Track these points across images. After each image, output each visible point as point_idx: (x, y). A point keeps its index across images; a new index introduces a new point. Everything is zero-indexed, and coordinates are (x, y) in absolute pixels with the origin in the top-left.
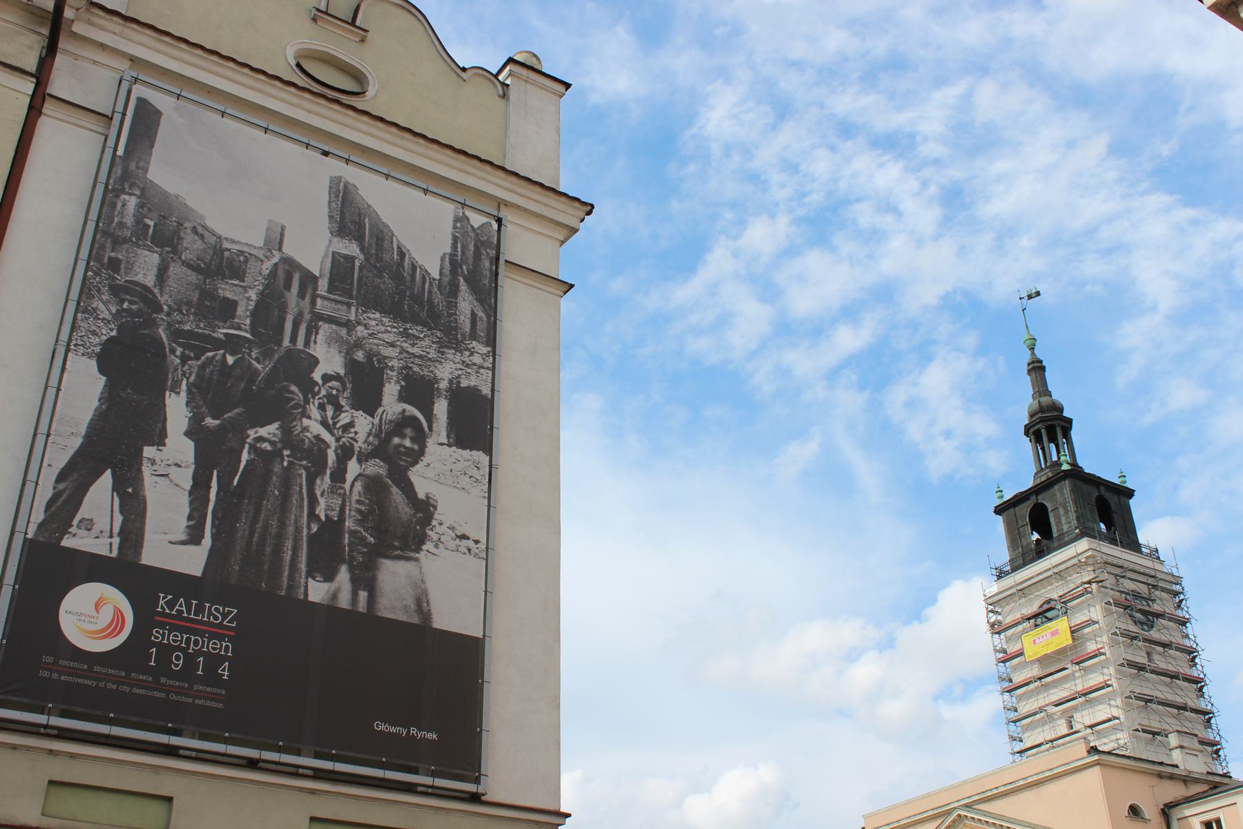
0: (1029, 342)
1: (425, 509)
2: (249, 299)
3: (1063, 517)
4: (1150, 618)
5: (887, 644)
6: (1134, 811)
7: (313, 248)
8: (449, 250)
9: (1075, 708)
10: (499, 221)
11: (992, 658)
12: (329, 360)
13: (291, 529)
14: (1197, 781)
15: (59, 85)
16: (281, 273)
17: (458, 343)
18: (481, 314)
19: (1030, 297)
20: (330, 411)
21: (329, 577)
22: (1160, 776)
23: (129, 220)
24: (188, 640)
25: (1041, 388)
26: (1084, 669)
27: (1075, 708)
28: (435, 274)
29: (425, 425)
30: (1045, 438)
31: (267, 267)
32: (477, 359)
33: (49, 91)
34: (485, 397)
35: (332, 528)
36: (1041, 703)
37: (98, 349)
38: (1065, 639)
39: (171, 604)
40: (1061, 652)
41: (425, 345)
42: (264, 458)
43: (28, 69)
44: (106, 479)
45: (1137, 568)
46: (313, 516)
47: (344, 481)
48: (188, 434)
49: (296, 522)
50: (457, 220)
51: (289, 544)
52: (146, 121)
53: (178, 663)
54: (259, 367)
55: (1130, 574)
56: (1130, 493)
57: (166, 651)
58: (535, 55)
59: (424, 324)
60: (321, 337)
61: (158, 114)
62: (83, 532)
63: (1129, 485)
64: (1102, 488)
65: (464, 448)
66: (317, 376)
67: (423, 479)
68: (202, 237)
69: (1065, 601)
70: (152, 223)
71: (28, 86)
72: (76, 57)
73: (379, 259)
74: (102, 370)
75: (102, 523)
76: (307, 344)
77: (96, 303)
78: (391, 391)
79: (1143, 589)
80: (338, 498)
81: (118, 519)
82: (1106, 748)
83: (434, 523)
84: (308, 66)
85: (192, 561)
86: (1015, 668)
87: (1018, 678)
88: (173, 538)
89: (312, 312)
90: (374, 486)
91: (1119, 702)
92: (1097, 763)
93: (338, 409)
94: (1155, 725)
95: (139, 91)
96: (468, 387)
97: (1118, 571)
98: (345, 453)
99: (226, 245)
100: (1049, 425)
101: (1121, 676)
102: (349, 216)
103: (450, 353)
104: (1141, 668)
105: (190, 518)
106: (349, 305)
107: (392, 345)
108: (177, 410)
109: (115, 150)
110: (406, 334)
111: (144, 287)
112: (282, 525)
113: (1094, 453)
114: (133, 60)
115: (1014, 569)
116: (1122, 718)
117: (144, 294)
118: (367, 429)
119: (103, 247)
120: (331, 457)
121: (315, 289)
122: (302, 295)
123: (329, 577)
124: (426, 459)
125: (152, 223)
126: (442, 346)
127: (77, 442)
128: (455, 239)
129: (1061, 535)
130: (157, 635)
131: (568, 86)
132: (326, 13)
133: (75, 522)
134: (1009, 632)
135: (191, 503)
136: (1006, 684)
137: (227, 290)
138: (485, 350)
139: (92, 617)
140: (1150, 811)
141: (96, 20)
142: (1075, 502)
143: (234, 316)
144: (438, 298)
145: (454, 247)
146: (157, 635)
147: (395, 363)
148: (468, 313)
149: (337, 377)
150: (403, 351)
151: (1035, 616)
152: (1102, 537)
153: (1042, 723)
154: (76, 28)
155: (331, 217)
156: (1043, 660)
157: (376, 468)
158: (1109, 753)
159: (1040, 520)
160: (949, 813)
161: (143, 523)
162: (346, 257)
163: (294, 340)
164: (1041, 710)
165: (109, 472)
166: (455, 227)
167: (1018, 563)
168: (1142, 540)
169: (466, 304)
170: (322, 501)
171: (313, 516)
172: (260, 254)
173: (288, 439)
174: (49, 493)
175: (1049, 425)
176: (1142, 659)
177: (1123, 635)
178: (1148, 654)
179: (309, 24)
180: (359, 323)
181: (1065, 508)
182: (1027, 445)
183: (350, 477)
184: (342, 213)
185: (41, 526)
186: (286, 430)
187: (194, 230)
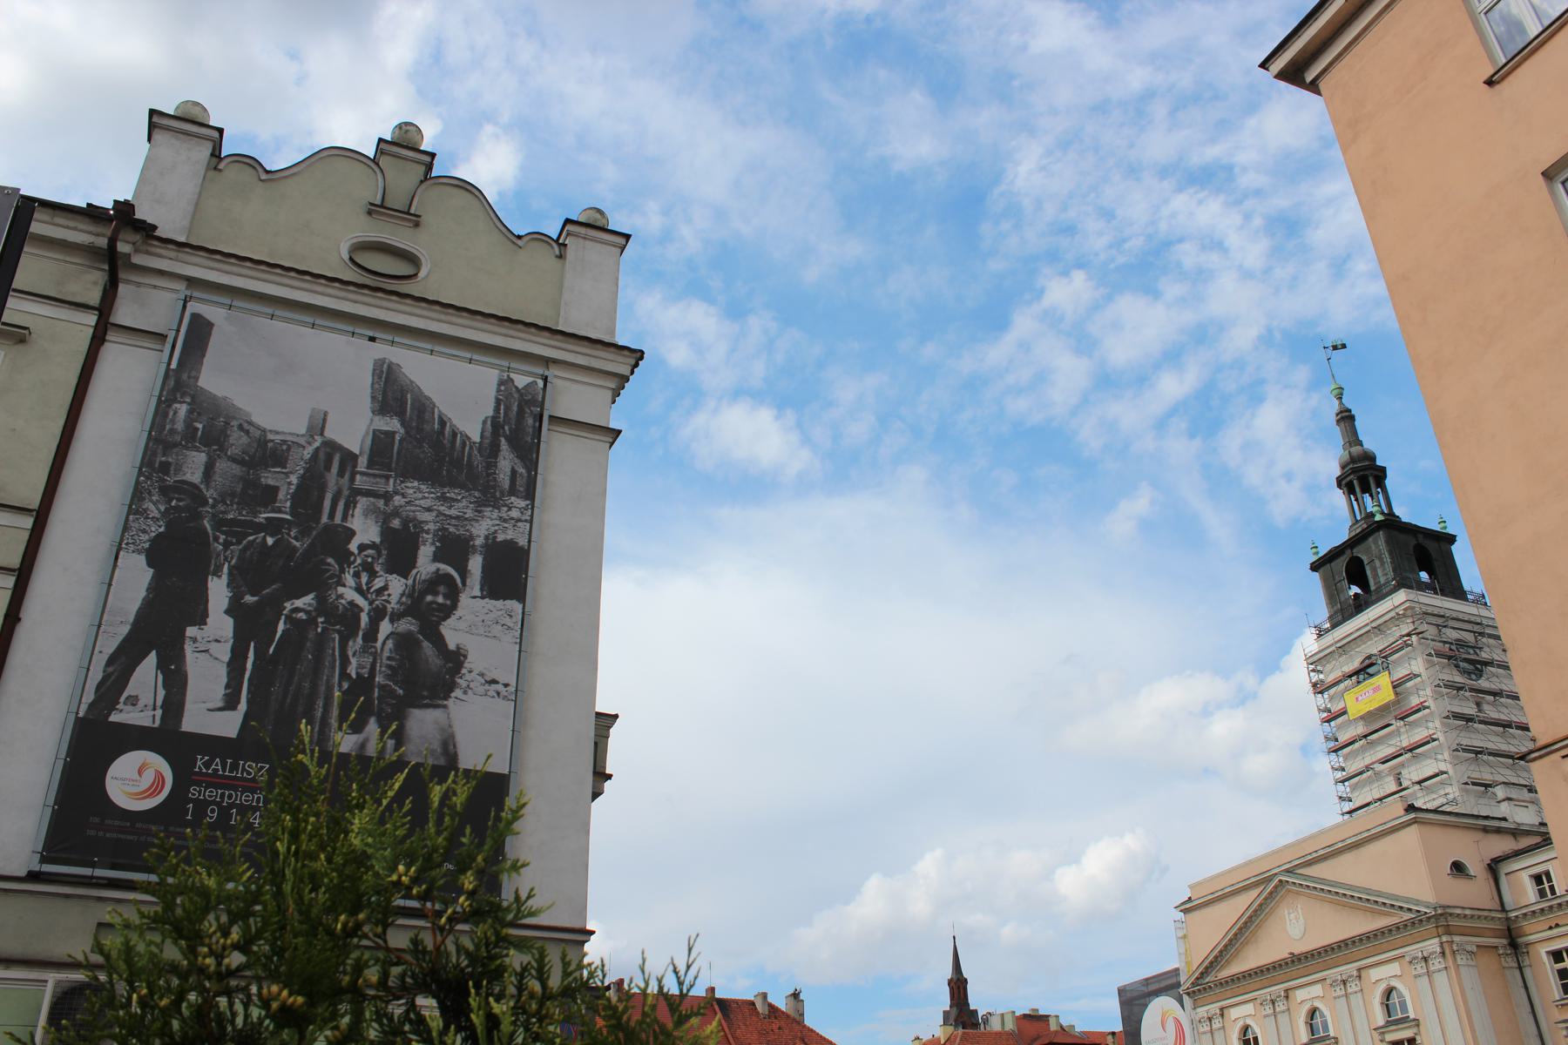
1: (456, 659)
2: (290, 483)
3: (1381, 570)
4: (1478, 667)
5: (1243, 698)
6: (1458, 868)
7: (353, 428)
8: (491, 413)
9: (1402, 765)
10: (545, 379)
11: (1317, 717)
12: (365, 530)
13: (323, 689)
14: (1528, 833)
15: (124, 314)
16: (322, 455)
17: (497, 500)
18: (522, 470)
19: (1335, 348)
20: (364, 578)
21: (357, 728)
22: (1485, 830)
23: (180, 426)
24: (223, 795)
25: (1352, 438)
26: (1410, 724)
27: (1402, 765)
28: (476, 438)
29: (458, 580)
30: (1358, 490)
31: (307, 453)
32: (515, 513)
33: (112, 320)
34: (522, 548)
35: (362, 685)
36: (1367, 761)
37: (147, 545)
38: (1387, 695)
39: (207, 765)
40: (1384, 709)
41: (463, 505)
42: (298, 628)
43: (91, 303)
44: (152, 658)
45: (1461, 616)
46: (344, 675)
47: (376, 640)
48: (227, 612)
49: (328, 681)
50: (501, 383)
51: (320, 703)
52: (199, 333)
53: (213, 815)
54: (297, 544)
55: (1451, 623)
56: (1451, 539)
57: (202, 806)
58: (598, 211)
59: (462, 486)
60: (358, 511)
61: (210, 325)
62: (129, 708)
63: (1450, 531)
64: (1420, 537)
65: (497, 599)
66: (353, 547)
67: (453, 633)
68: (247, 432)
69: (1385, 655)
70: (200, 426)
71: (91, 319)
72: (139, 284)
73: (420, 430)
74: (149, 564)
75: (146, 698)
76: (345, 518)
77: (148, 505)
78: (426, 552)
79: (1470, 637)
80: (367, 657)
81: (161, 693)
82: (1430, 806)
83: (464, 671)
84: (363, 259)
85: (228, 725)
86: (1339, 727)
87: (1344, 737)
88: (211, 705)
89: (350, 488)
90: (404, 643)
91: (1446, 755)
92: (1414, 821)
93: (373, 575)
94: (1487, 777)
95: (193, 307)
96: (505, 541)
97: (1440, 621)
98: (378, 615)
99: (270, 437)
100: (1363, 475)
101: (1447, 729)
102: (391, 393)
103: (487, 511)
104: (1469, 719)
105: (227, 687)
106: (387, 478)
107: (429, 510)
108: (218, 591)
109: (169, 364)
110: (443, 498)
111: (195, 486)
112: (314, 686)
113: (1412, 501)
114: (191, 282)
115: (1334, 626)
116: (1451, 772)
117: (192, 492)
118: (400, 591)
119: (154, 454)
120: (364, 618)
121: (355, 466)
122: (341, 474)
123: (357, 728)
124: (458, 613)
125: (200, 426)
126: (480, 505)
127: (126, 629)
128: (498, 402)
129: (1379, 588)
130: (194, 792)
131: (628, 237)
132: (382, 206)
133: (122, 699)
134: (1332, 691)
135: (229, 673)
136: (1332, 744)
137: (269, 478)
138: (523, 504)
139: (135, 781)
140: (1475, 866)
141: (153, 250)
142: (1391, 553)
143: (275, 501)
144: (478, 460)
145: (497, 409)
146: (194, 792)
147: (431, 527)
148: (508, 470)
149: (373, 546)
150: (440, 513)
151: (1357, 673)
152: (1421, 587)
153: (1369, 781)
154: (138, 259)
155: (373, 398)
156: (1367, 717)
157: (407, 625)
158: (1435, 811)
159: (1357, 574)
160: (1269, 879)
161: (184, 694)
162: (386, 433)
163: (332, 515)
164: (1368, 768)
165: (154, 653)
166: (499, 391)
168: (1466, 587)
169: (506, 462)
170: (354, 661)
171: (344, 675)
172: (302, 441)
173: (323, 607)
174: (100, 676)
175: (1363, 475)
176: (1469, 709)
177: (1446, 686)
178: (1478, 704)
179: (364, 218)
180: (396, 493)
181: (1381, 559)
182: (1339, 498)
183: (381, 637)
184: (385, 393)
185: (91, 706)
186: (321, 599)
187: (241, 427)
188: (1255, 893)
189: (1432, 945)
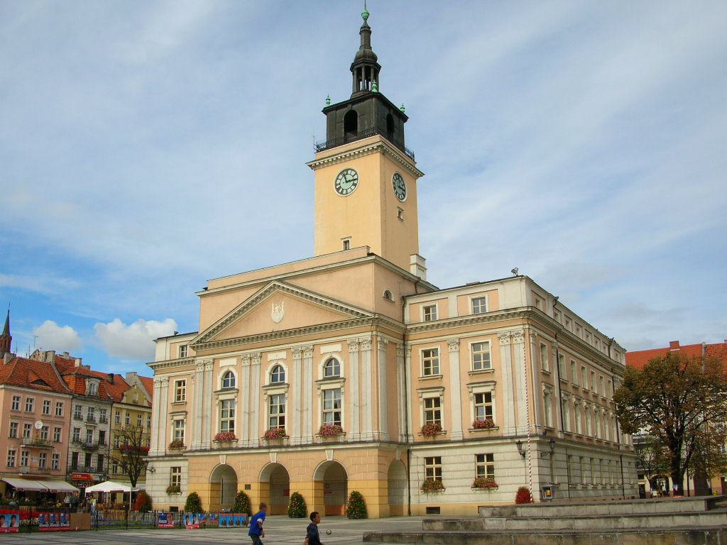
0: (364, 15)
6: (387, 295)
25: (366, 43)
56: (405, 119)
64: (392, 111)
100: (366, 67)
113: (389, 86)
115: (327, 148)
160: (268, 282)
167: (332, 143)
175: (366, 67)
182: (349, 78)
188: (253, 291)
189: (367, 336)
